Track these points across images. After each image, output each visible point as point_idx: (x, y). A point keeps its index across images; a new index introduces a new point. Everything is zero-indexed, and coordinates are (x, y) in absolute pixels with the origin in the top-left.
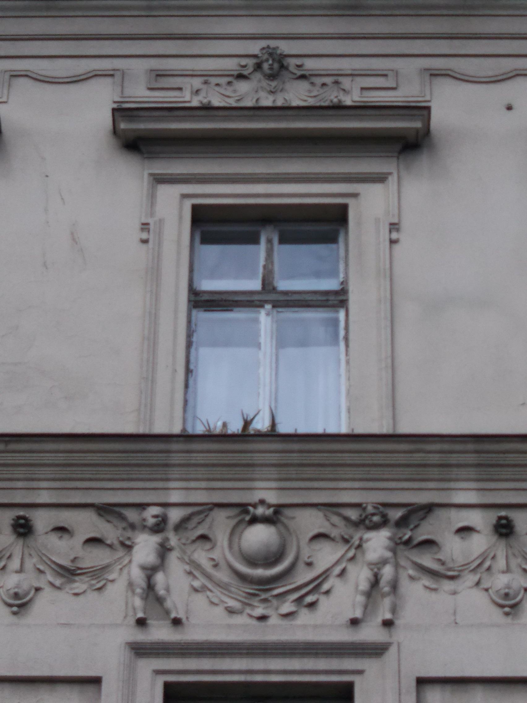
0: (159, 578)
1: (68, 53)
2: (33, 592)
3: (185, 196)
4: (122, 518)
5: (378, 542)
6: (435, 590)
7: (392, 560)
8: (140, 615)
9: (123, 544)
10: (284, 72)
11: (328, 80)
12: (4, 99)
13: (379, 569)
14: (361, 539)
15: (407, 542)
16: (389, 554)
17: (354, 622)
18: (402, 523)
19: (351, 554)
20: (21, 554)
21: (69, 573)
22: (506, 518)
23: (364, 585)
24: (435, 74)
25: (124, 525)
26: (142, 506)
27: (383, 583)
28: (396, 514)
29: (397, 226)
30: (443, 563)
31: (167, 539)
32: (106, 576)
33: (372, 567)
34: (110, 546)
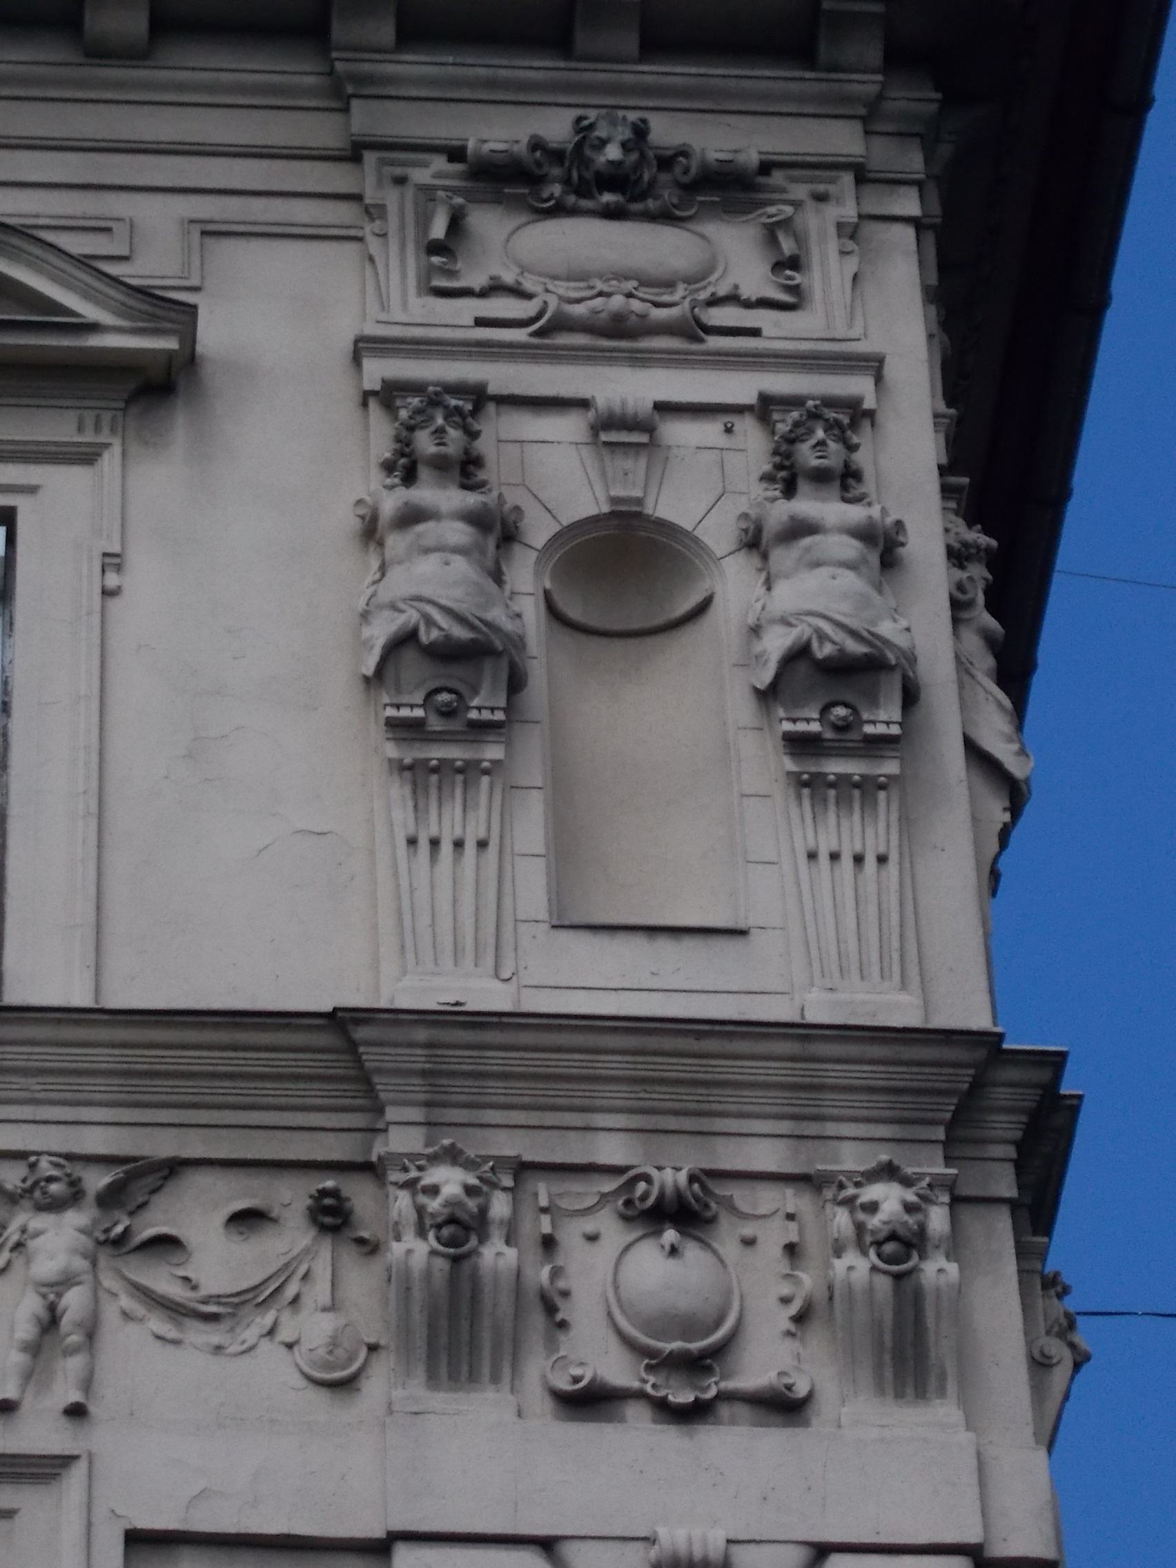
2: (363, 1353)
5: (58, 1240)
6: (176, 1342)
7: (88, 1277)
12: (194, 282)
13: (59, 1295)
14: (24, 1230)
15: (118, 1242)
16: (80, 1264)
18: (110, 1199)
20: (329, 1270)
22: (334, 1193)
23: (26, 1330)
24: (212, 232)
27: (65, 1323)
28: (97, 1180)
33: (44, 1290)
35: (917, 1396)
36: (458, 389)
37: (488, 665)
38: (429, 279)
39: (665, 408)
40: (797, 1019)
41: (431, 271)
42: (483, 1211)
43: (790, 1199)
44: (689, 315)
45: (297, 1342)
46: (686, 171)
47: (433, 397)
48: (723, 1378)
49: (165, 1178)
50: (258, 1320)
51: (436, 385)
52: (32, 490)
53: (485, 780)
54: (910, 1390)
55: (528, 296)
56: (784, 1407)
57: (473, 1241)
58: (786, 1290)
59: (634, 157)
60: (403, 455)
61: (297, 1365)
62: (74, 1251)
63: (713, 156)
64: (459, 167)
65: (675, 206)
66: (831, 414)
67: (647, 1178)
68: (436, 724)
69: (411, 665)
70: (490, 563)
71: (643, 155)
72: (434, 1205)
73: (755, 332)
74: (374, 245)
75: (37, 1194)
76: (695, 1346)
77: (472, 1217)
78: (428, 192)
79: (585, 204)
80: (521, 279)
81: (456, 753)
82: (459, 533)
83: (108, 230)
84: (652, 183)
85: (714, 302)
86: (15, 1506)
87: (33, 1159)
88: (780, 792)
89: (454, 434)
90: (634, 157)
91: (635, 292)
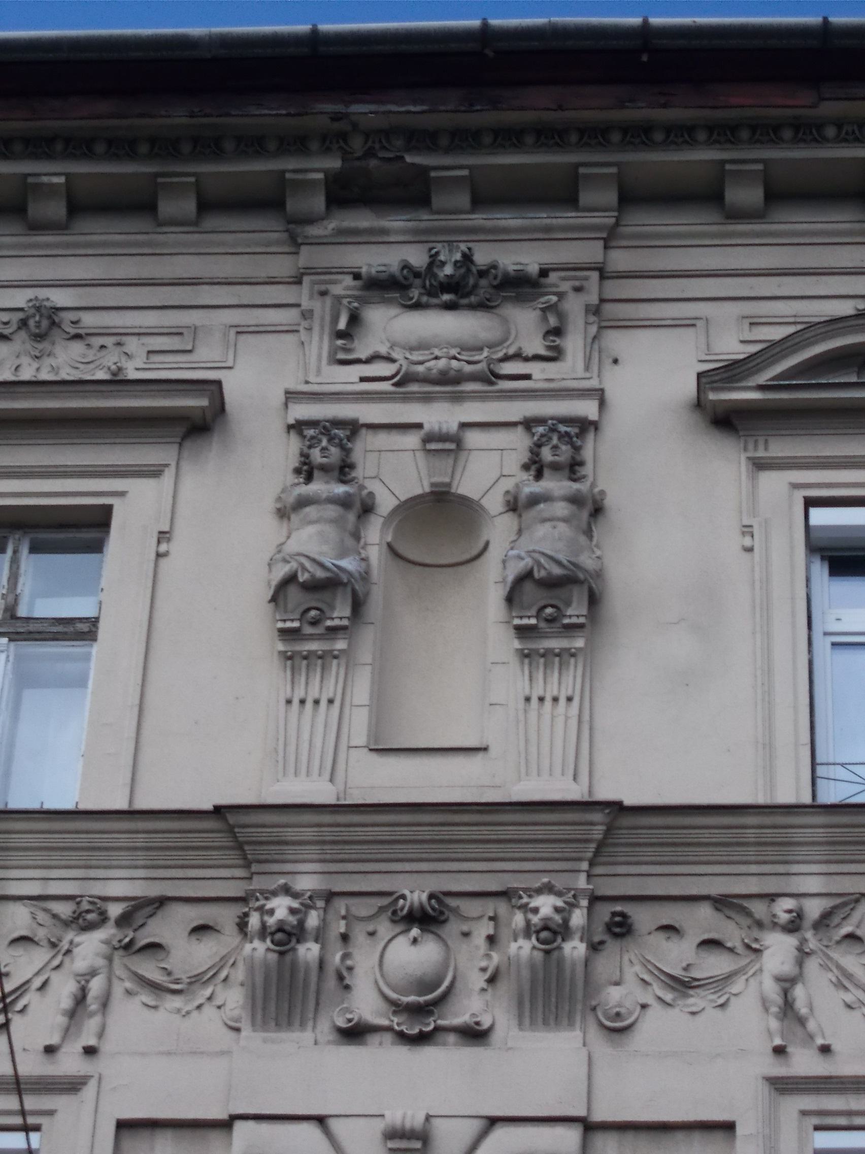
0: (799, 992)
1: (708, 295)
2: (639, 1008)
3: (796, 486)
4: (748, 913)
5: (90, 947)
6: (155, 1007)
7: (105, 970)
8: (778, 1041)
9: (748, 947)
10: (55, 331)
11: (109, 341)
12: (230, 364)
13: (88, 981)
14: (71, 942)
15: (127, 947)
16: (101, 962)
17: (50, 1050)
18: (124, 921)
19: (56, 962)
21: (683, 985)
22: (623, 915)
23: (67, 1003)
25: (749, 921)
26: (772, 897)
28: (115, 910)
29: (168, 535)
30: (169, 974)
31: (804, 941)
32: (727, 989)
33: (79, 978)
34: (731, 950)
35: (556, 1024)
36: (338, 423)
37: (340, 592)
38: (336, 353)
39: (464, 426)
40: (586, 798)
41: (333, 351)
42: (566, 922)
43: (490, 907)
44: (486, 370)
45: (224, 1005)
46: (495, 278)
47: (328, 427)
48: (439, 1018)
49: (157, 908)
50: (202, 992)
51: (552, 419)
52: (122, 494)
53: (335, 662)
54: (552, 1022)
55: (393, 361)
56: (475, 1035)
57: (559, 940)
58: (483, 964)
59: (463, 271)
60: (305, 464)
61: (226, 1024)
62: (97, 954)
63: (511, 268)
64: (358, 283)
65: (488, 300)
66: (562, 428)
67: (403, 897)
68: (308, 630)
69: (293, 594)
70: (584, 525)
71: (469, 270)
72: (535, 919)
73: (528, 377)
74: (303, 335)
75: (81, 921)
76: (422, 999)
77: (559, 925)
78: (338, 299)
79: (434, 301)
80: (391, 352)
81: (555, 644)
82: (561, 509)
83: (181, 334)
84: (475, 286)
85: (506, 358)
86: (53, 1107)
87: (79, 899)
88: (514, 661)
89: (334, 450)
90: (463, 271)
91: (458, 356)
